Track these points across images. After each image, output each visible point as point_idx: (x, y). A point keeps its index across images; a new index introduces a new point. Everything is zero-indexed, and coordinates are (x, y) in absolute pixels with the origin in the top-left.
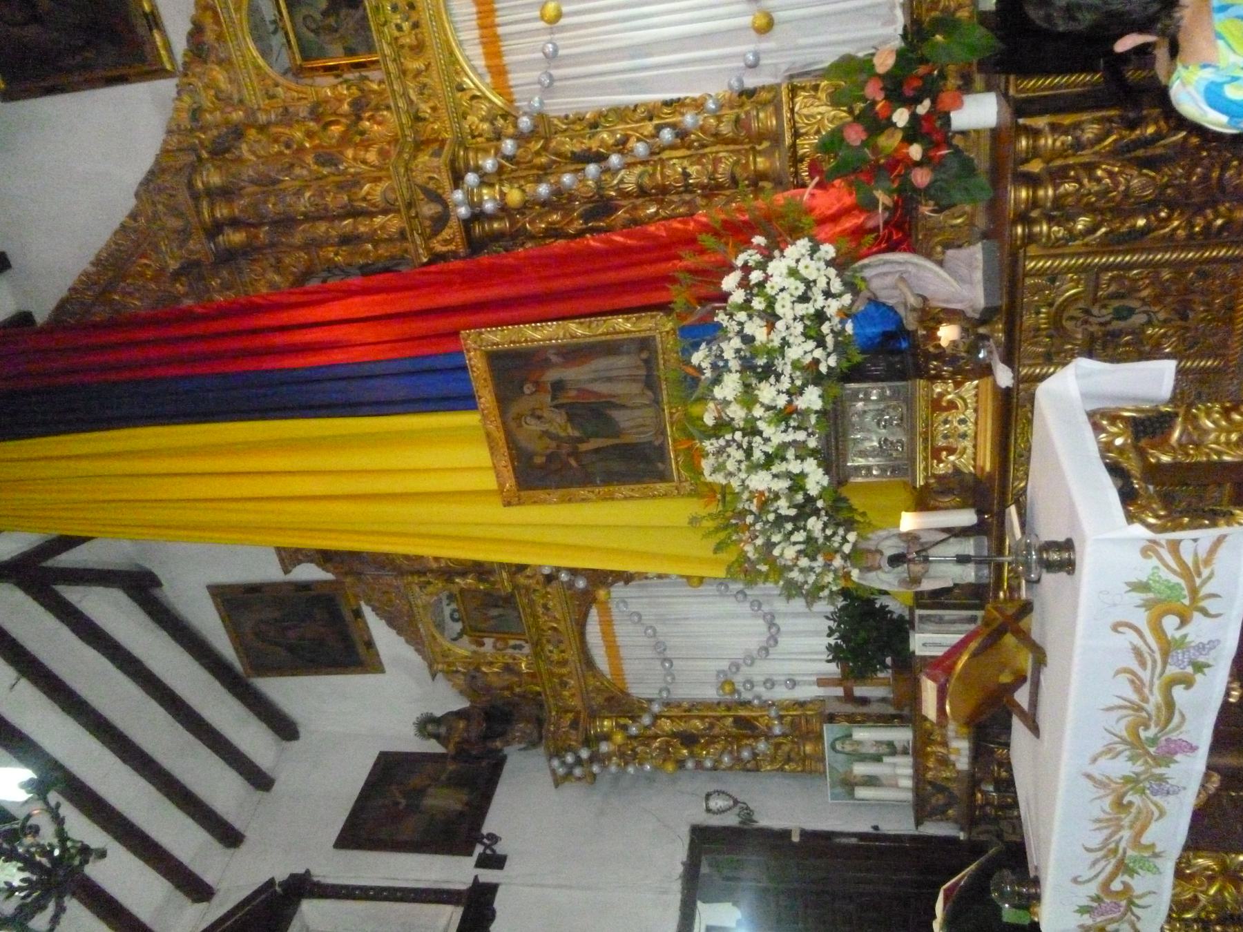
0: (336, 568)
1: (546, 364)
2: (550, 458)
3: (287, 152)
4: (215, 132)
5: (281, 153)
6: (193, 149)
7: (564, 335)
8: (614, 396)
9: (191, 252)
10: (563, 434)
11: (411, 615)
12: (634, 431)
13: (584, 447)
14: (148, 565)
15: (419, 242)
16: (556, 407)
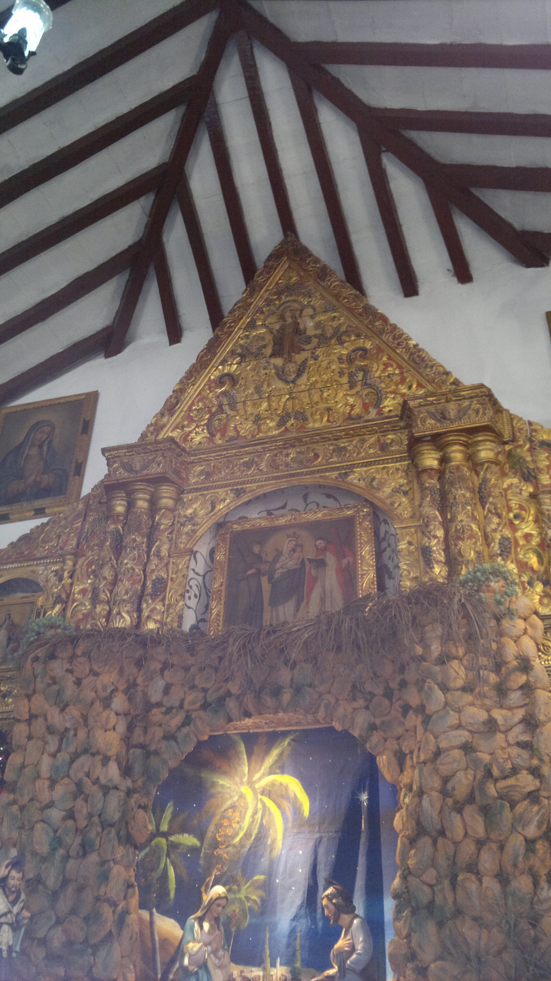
0: (95, 497)
1: (340, 555)
2: (259, 558)
3: (511, 515)
4: (529, 459)
5: (510, 510)
6: (514, 440)
7: (364, 570)
8: (307, 603)
9: (424, 421)
10: (278, 565)
11: (30, 558)
12: (274, 615)
13: (264, 580)
14: (127, 351)
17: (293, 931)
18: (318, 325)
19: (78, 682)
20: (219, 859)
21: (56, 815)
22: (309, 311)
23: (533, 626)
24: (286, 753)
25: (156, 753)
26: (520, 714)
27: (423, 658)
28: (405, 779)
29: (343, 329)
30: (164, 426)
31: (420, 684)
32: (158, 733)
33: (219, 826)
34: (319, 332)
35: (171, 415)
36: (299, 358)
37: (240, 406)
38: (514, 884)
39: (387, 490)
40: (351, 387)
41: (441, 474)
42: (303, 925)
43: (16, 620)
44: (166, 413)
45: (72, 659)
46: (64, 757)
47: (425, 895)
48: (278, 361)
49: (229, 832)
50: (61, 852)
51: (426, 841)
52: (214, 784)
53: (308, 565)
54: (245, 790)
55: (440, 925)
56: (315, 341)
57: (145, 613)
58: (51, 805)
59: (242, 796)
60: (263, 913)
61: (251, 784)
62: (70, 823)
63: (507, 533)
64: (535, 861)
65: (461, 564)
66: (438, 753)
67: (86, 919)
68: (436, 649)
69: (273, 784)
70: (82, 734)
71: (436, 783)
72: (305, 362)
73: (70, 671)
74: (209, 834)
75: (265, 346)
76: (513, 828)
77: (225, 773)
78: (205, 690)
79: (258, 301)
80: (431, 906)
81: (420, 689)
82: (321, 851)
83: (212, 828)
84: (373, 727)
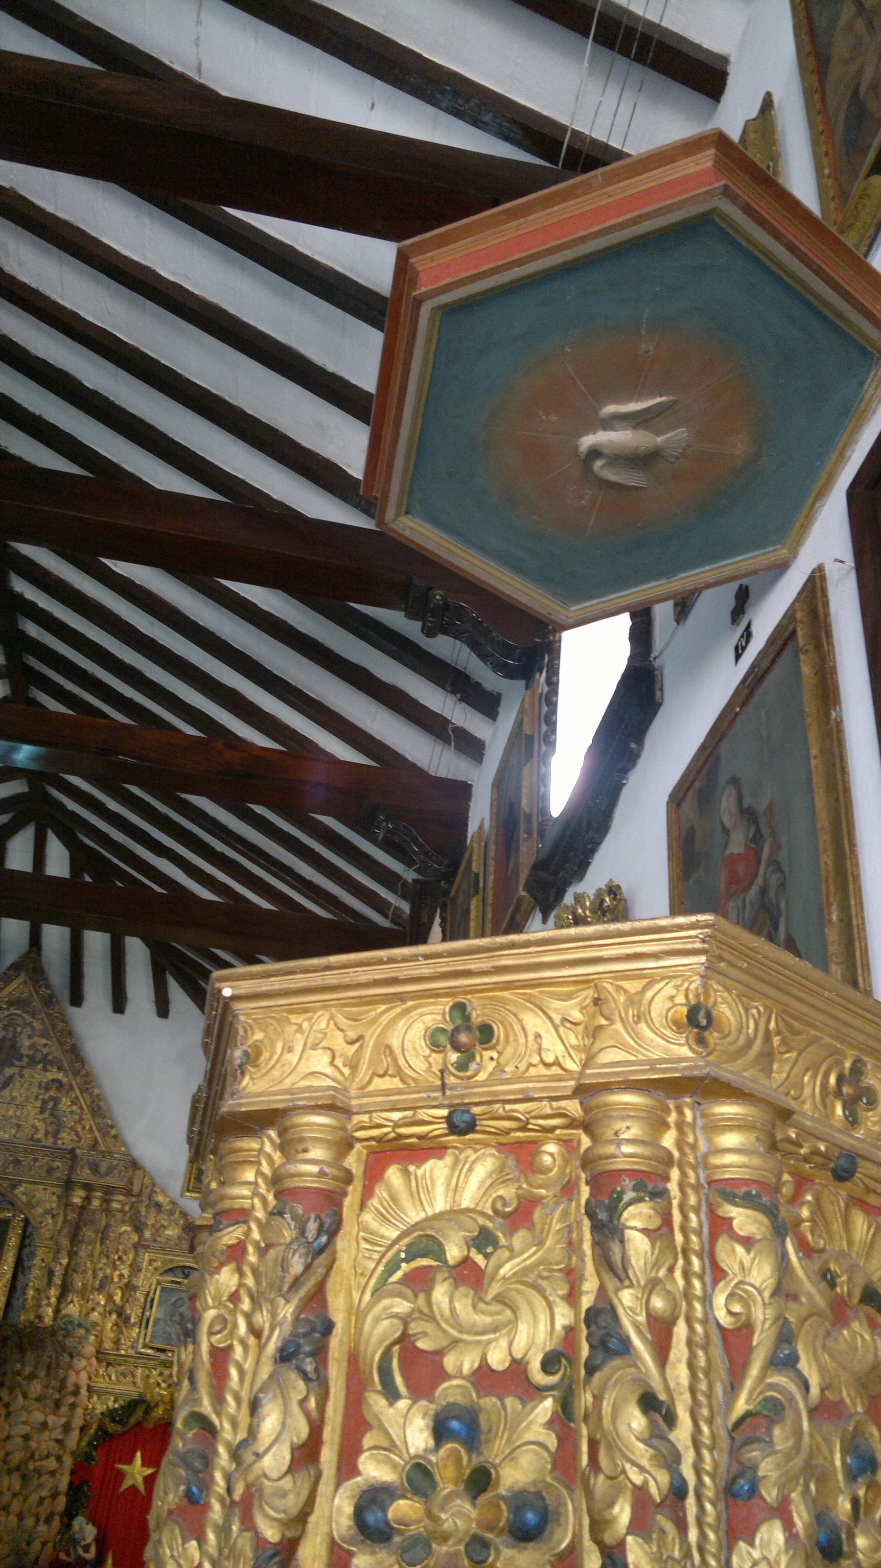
6: (139, 1195)
15: (50, 1311)
18: (32, 1047)
22: (28, 1030)
23: (90, 1365)
26: (63, 1420)
27: (19, 1373)
29: (50, 1058)
31: (12, 1389)
34: (31, 1053)
38: (25, 1521)
39: (40, 1210)
40: (41, 1112)
41: (83, 1208)
56: (26, 1060)
63: (108, 1271)
65: (69, 1291)
66: (9, 1437)
68: (28, 1370)
76: (35, 1490)
81: (11, 1393)
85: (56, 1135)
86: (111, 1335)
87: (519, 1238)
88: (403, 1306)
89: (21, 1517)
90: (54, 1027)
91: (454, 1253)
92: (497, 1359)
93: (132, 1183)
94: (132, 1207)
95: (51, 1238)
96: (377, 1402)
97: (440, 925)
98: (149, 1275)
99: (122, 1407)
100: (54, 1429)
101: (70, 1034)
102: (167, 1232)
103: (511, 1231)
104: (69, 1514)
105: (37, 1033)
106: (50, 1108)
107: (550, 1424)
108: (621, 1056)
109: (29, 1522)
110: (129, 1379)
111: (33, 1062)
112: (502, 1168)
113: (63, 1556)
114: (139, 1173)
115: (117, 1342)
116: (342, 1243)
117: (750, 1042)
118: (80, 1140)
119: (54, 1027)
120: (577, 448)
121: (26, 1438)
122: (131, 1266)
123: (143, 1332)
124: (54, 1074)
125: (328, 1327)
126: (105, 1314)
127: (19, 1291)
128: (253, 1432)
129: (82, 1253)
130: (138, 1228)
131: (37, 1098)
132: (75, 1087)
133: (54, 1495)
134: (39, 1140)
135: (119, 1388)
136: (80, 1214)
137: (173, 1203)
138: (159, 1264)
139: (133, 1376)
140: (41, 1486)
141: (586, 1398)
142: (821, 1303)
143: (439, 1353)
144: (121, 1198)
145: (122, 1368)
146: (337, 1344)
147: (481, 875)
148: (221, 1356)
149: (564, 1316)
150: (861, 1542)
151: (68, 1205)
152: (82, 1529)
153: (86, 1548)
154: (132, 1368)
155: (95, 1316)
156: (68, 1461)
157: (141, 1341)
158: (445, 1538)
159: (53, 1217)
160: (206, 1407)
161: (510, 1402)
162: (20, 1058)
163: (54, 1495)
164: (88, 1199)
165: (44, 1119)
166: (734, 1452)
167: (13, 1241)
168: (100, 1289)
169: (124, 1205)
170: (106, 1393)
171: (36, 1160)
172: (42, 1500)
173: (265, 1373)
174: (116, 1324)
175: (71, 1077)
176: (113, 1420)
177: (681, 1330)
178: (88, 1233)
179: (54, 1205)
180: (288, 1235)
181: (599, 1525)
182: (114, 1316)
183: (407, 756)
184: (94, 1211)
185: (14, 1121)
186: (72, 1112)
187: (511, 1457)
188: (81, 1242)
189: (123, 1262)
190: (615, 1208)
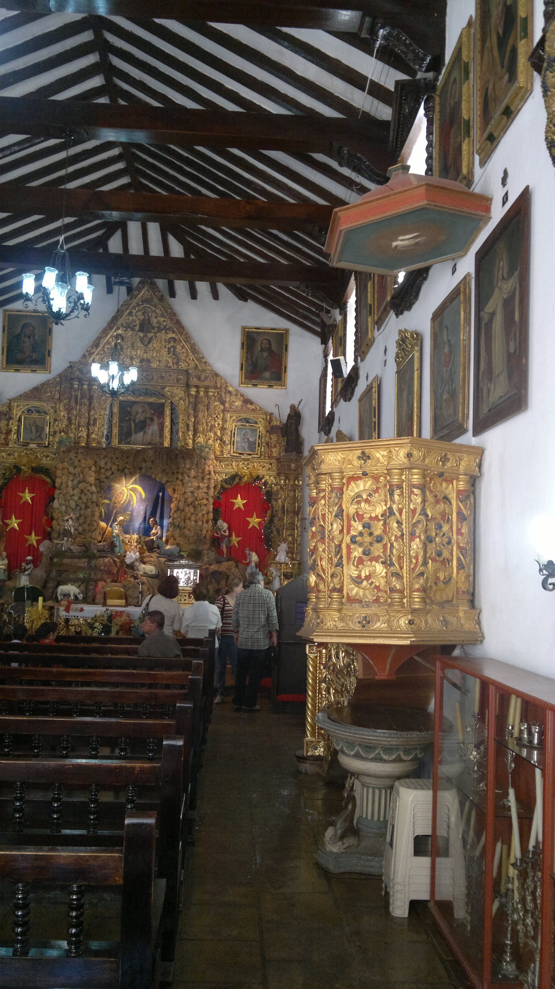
1: (159, 418)
6: (221, 388)
10: (137, 417)
13: (132, 422)
15: (191, 441)
16: (146, 418)
17: (139, 528)
18: (158, 322)
19: (79, 461)
20: (116, 507)
21: (76, 498)
22: (154, 314)
24: (138, 479)
25: (103, 482)
26: (206, 485)
28: (175, 496)
29: (167, 327)
30: (93, 353)
32: (104, 476)
33: (116, 498)
34: (158, 325)
35: (97, 348)
36: (150, 335)
37: (125, 350)
40: (169, 354)
41: (196, 396)
42: (142, 526)
43: (39, 424)
44: (94, 347)
45: (77, 453)
46: (75, 482)
47: (177, 523)
48: (142, 335)
49: (119, 500)
50: (79, 508)
51: (179, 512)
52: (114, 486)
53: (148, 420)
54: (124, 488)
55: (180, 530)
56: (156, 329)
57: (91, 431)
58: (73, 495)
59: (123, 490)
60: (130, 522)
61: (126, 487)
62: (80, 501)
63: (213, 423)
64: (204, 519)
66: (185, 493)
67: (89, 525)
68: (188, 466)
69: (133, 488)
70: (81, 476)
71: (183, 499)
72: (152, 337)
73: (76, 457)
74: (113, 500)
75: (135, 326)
77: (117, 483)
78: (118, 465)
79: (135, 302)
80: (178, 526)
81: (183, 476)
82: (148, 508)
83: (114, 498)
84: (167, 482)
85: (177, 363)
86: (219, 449)
87: (376, 495)
88: (356, 507)
89: (196, 521)
90: (166, 312)
91: (365, 497)
92: (373, 515)
93: (216, 383)
94: (218, 393)
95: (185, 410)
96: (353, 522)
97: (355, 280)
98: (231, 423)
99: (229, 478)
100: (202, 489)
101: (175, 314)
102: (236, 404)
103: (375, 494)
104: (215, 520)
105: (159, 315)
106: (172, 351)
107: (382, 525)
108: (395, 462)
109: (200, 523)
110: (230, 467)
111: (160, 330)
112: (373, 483)
113: (215, 535)
114: (219, 379)
115: (222, 452)
116: (344, 496)
117: (420, 457)
118: (189, 365)
119: (166, 312)
120: (391, 245)
121: (192, 492)
122: (222, 419)
123: (232, 447)
124: (171, 335)
125: (343, 511)
126: (214, 441)
127: (174, 433)
128: (332, 529)
129: (200, 416)
130: (223, 403)
131: (165, 347)
132: (182, 340)
133: (208, 513)
134: (170, 367)
135: (227, 470)
136: (196, 398)
137: (236, 390)
138: (234, 418)
139: (232, 465)
140: (202, 510)
141: (388, 521)
142: (433, 501)
143: (363, 514)
144: (213, 390)
145: (226, 463)
146: (344, 513)
147: (372, 305)
148: (324, 515)
149: (384, 508)
150: (437, 539)
151: (189, 395)
152: (221, 525)
153: (225, 531)
154: (231, 462)
155: (210, 442)
156: (211, 501)
157: (232, 450)
158: (366, 542)
159: (183, 401)
160: (322, 523)
161: (376, 522)
162: (154, 328)
163: (208, 513)
164: (198, 392)
165: (171, 357)
166: (413, 528)
167: (168, 412)
168: (211, 431)
169: (214, 393)
170: (221, 473)
171: (171, 376)
172: (203, 515)
173: (333, 519)
174: (220, 444)
175: (179, 335)
176: (226, 483)
177: (404, 510)
178: (201, 407)
179: (183, 395)
180: (334, 495)
181: (390, 540)
182: (219, 441)
183: (333, 192)
184: (202, 397)
185: (157, 358)
186: (183, 353)
187: (376, 530)
188: (198, 411)
189: (218, 418)
190: (393, 491)
